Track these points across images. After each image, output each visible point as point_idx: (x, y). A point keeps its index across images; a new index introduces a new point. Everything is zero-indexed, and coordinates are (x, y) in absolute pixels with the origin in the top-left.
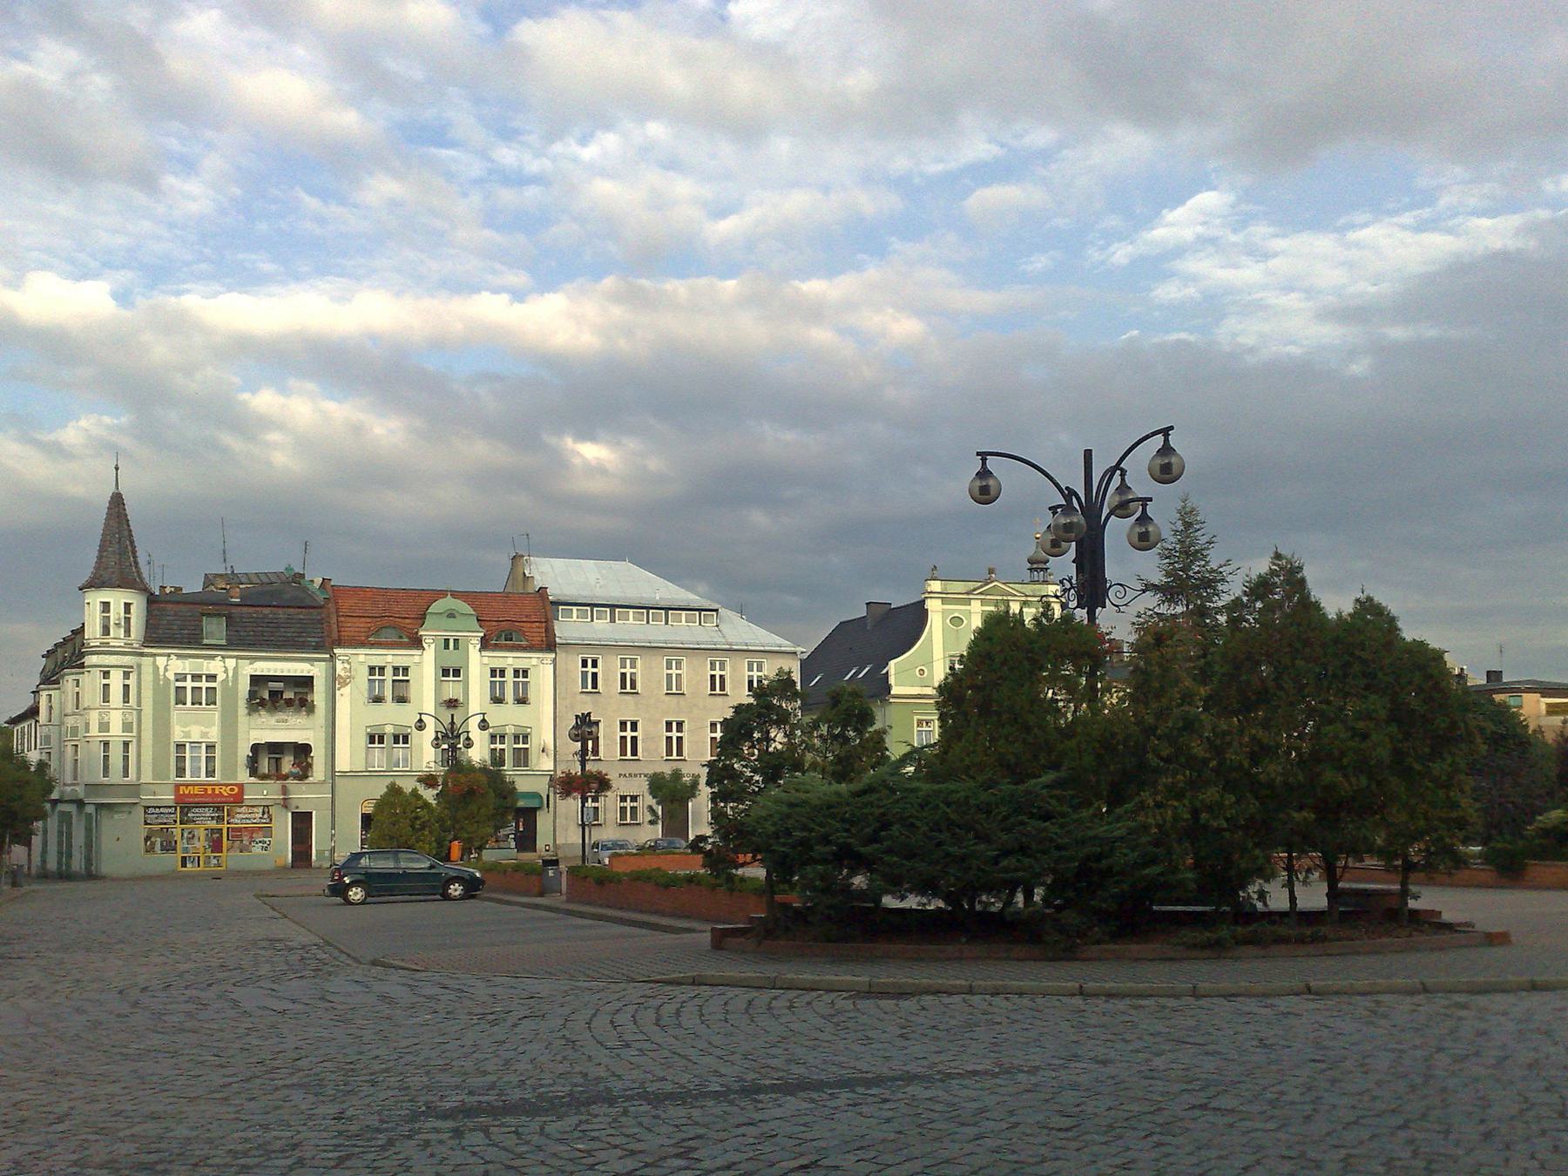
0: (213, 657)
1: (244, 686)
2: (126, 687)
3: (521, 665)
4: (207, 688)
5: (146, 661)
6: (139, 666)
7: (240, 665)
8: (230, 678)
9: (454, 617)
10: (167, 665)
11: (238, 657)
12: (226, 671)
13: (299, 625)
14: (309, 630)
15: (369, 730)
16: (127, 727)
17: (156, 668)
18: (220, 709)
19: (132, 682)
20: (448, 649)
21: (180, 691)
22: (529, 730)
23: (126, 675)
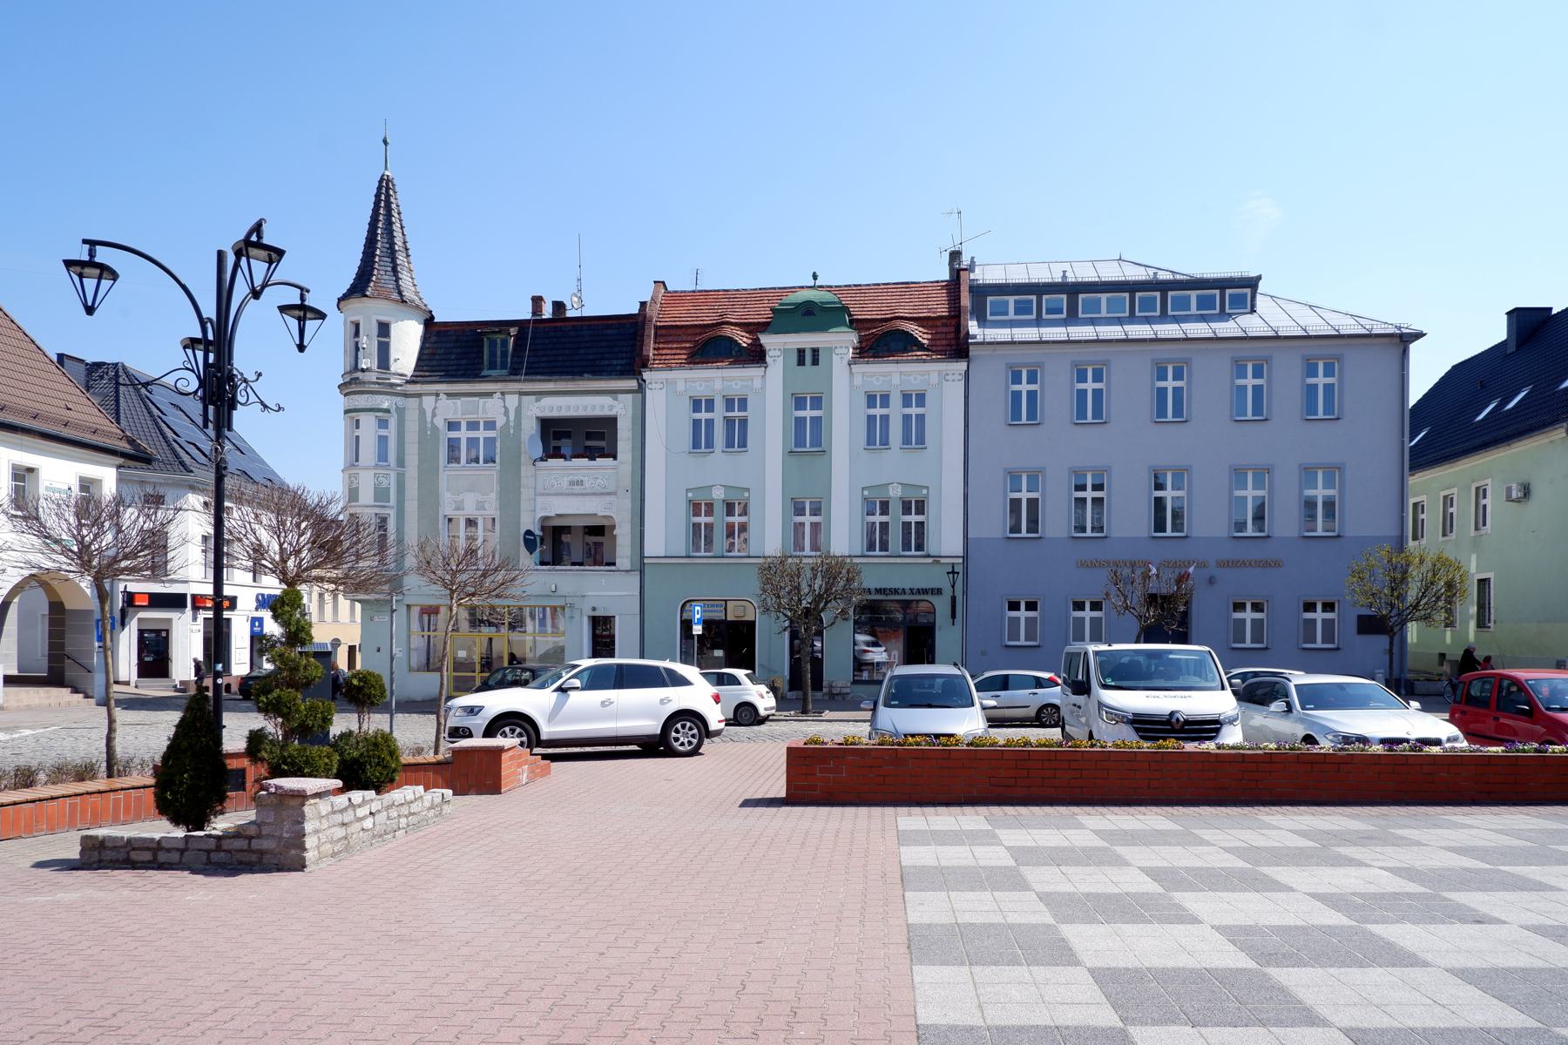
0: (489, 394)
1: (530, 428)
2: (383, 440)
3: (914, 385)
4: (1021, 491)
5: (412, 403)
6: (401, 412)
7: (524, 404)
8: (512, 424)
9: (813, 314)
10: (435, 408)
11: (522, 394)
12: (506, 413)
13: (605, 344)
14: (616, 349)
15: (690, 495)
16: (381, 494)
17: (422, 412)
18: (498, 468)
19: (391, 432)
20: (1076, 490)
21: (453, 445)
22: (925, 491)
23: (383, 424)
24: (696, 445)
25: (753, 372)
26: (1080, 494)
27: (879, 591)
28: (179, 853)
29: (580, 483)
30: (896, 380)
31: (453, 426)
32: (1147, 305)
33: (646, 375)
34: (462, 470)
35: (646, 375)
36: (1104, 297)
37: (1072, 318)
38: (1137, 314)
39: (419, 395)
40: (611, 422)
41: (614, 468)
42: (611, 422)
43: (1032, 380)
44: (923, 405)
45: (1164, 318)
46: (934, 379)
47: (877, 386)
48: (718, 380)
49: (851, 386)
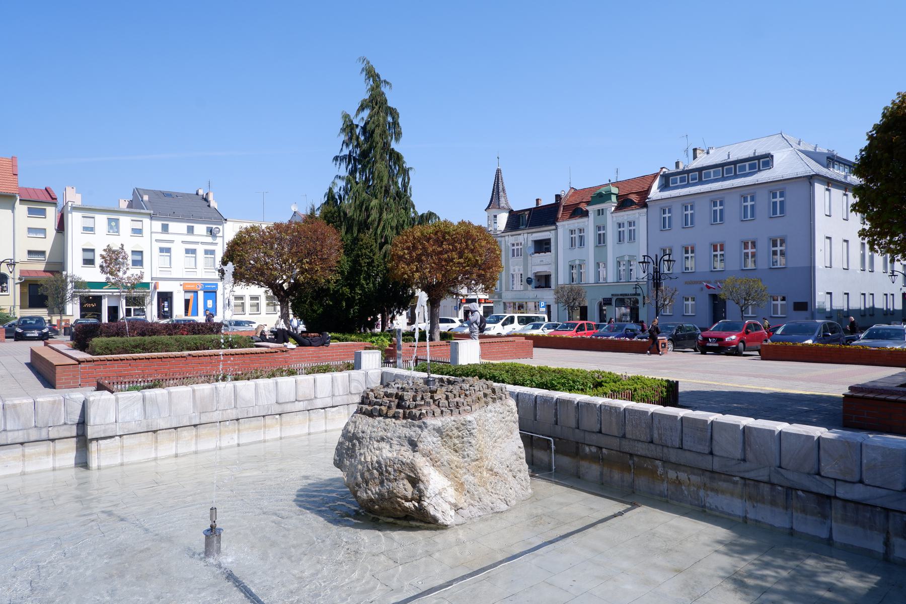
0: (520, 234)
1: (530, 244)
11: (528, 233)
24: (620, 241)
25: (585, 219)
26: (722, 253)
27: (621, 295)
28: (743, 458)
29: (542, 261)
30: (626, 218)
31: (513, 245)
32: (729, 171)
33: (557, 224)
34: (516, 259)
35: (557, 224)
36: (712, 171)
37: (701, 182)
38: (738, 173)
39: (505, 236)
40: (549, 240)
41: (550, 255)
42: (549, 240)
43: (752, 200)
44: (634, 226)
45: (736, 176)
46: (637, 215)
47: (620, 220)
48: (576, 223)
49: (613, 221)
